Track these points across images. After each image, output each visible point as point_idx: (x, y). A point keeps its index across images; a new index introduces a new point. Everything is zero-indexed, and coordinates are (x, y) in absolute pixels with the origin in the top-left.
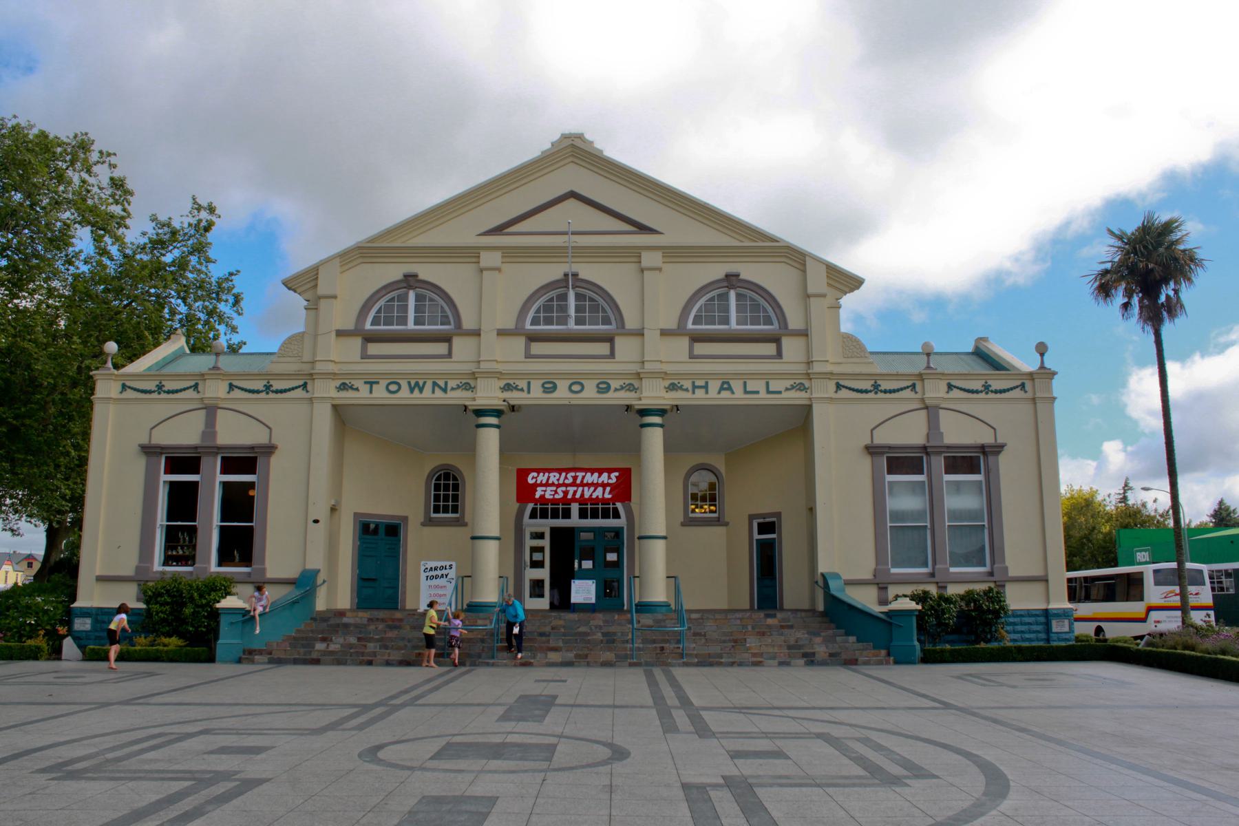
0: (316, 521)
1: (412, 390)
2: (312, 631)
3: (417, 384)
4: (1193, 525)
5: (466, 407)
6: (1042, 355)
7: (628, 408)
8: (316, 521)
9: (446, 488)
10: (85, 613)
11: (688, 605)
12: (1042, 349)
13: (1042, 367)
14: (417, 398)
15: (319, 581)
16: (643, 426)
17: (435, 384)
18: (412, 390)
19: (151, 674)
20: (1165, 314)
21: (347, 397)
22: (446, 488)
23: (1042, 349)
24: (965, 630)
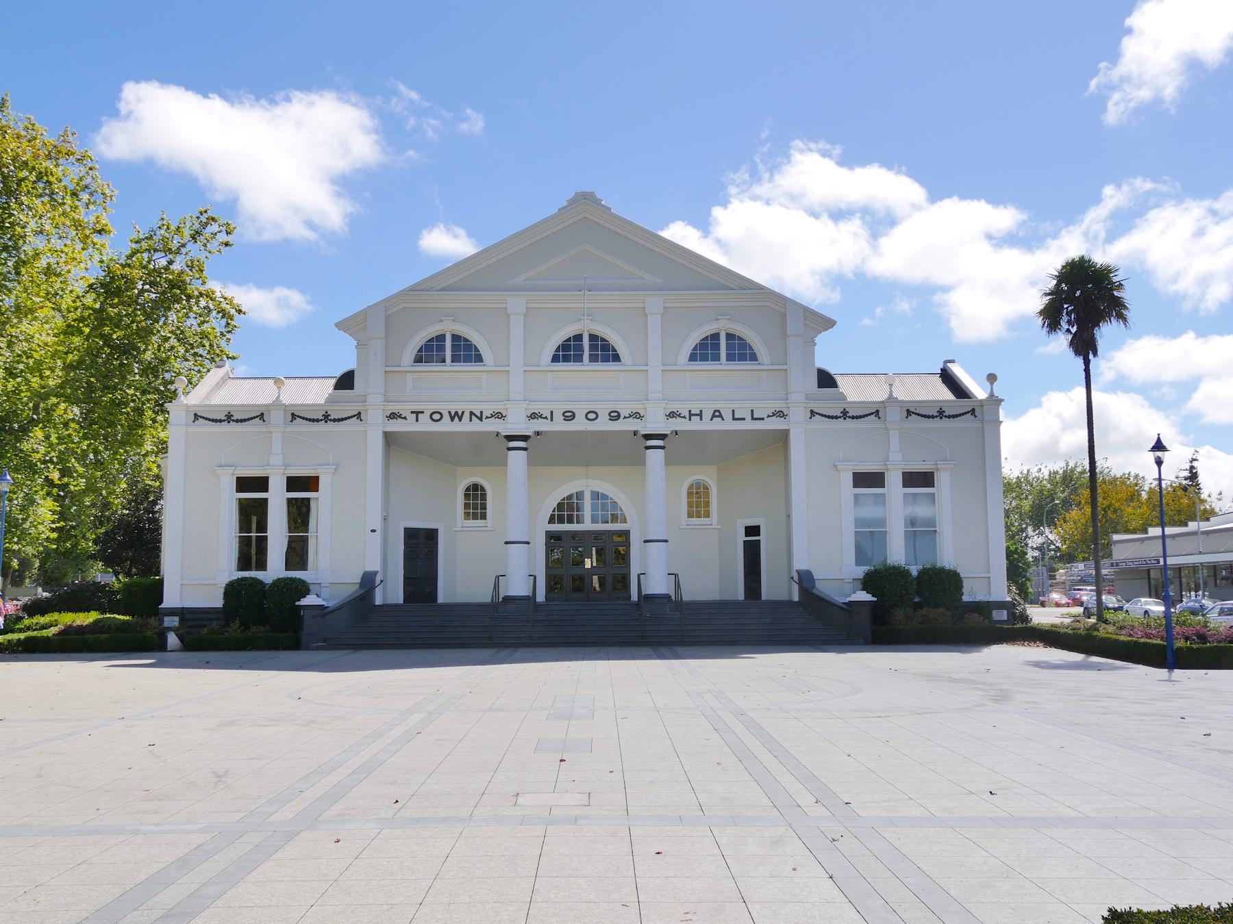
0: (373, 531)
1: (452, 419)
2: (35, 608)
3: (456, 413)
4: (1005, 218)
5: (498, 434)
6: (992, 384)
7: (635, 433)
8: (373, 531)
9: (475, 497)
10: (172, 612)
11: (687, 597)
12: (992, 378)
13: (992, 395)
14: (456, 427)
15: (378, 581)
16: (648, 448)
17: (472, 413)
18: (452, 419)
19: (1099, 668)
20: (1144, 495)
21: (396, 426)
22: (475, 497)
23: (992, 378)
24: (910, 609)
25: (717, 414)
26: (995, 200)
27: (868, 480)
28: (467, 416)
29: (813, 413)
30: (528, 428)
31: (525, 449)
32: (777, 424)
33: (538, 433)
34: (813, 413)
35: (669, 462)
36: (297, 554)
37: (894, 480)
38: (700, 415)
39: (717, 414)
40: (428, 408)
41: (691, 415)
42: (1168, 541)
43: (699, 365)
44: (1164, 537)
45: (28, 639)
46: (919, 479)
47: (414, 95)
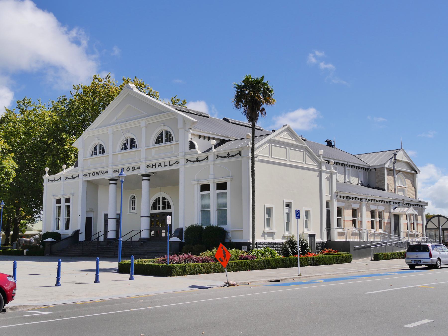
25: (160, 165)
26: (306, 108)
27: (205, 188)
28: (157, 165)
29: (187, 161)
30: (150, 170)
31: (116, 184)
32: (175, 167)
33: (153, 173)
34: (187, 161)
35: (151, 186)
36: (118, 231)
37: (213, 187)
38: (155, 166)
39: (160, 165)
40: (131, 166)
41: (153, 166)
42: (101, 274)
43: (159, 145)
44: (97, 271)
45: (267, 214)
46: (222, 186)
47: (381, 119)
